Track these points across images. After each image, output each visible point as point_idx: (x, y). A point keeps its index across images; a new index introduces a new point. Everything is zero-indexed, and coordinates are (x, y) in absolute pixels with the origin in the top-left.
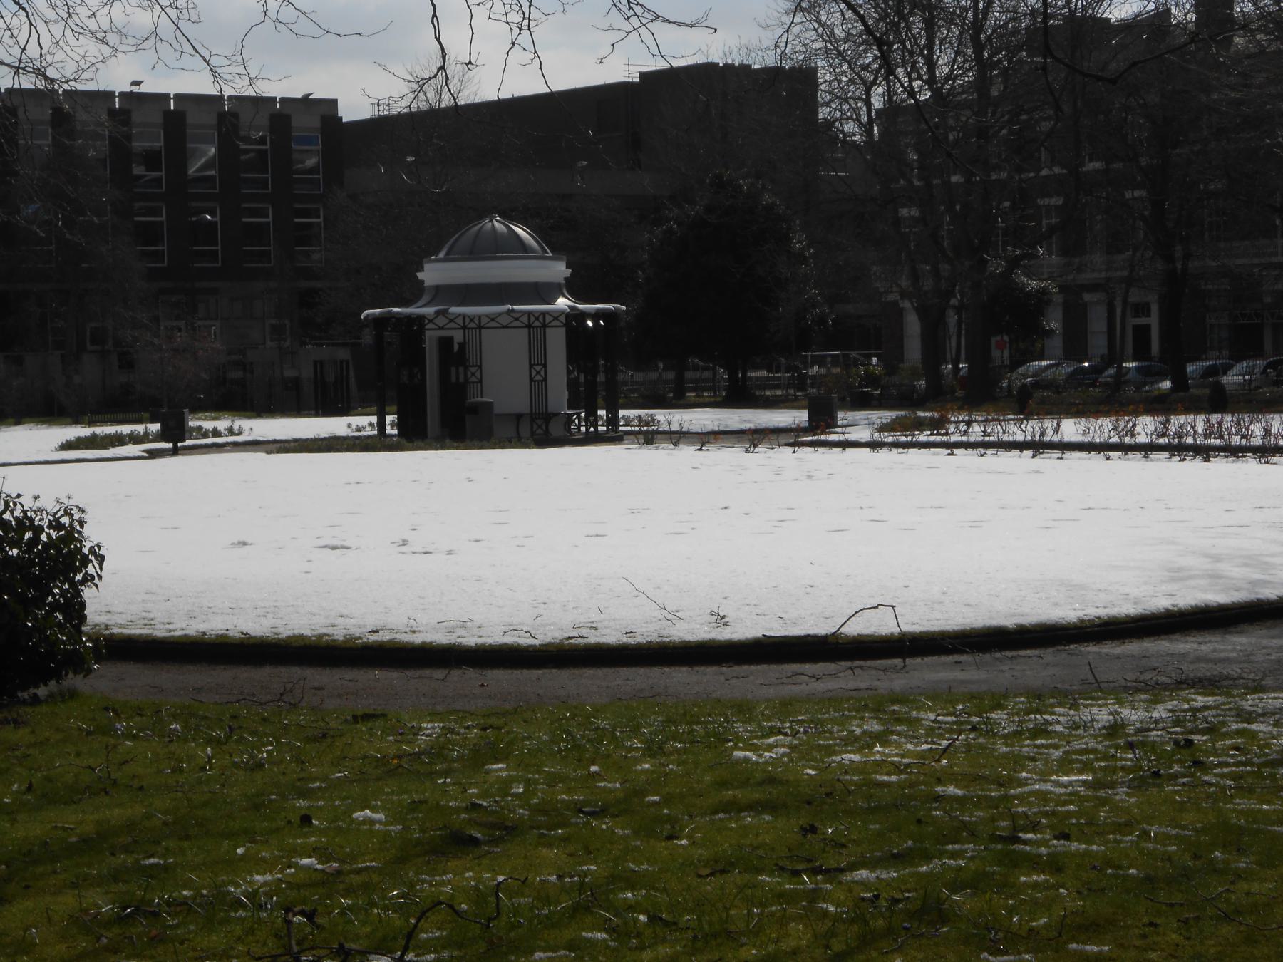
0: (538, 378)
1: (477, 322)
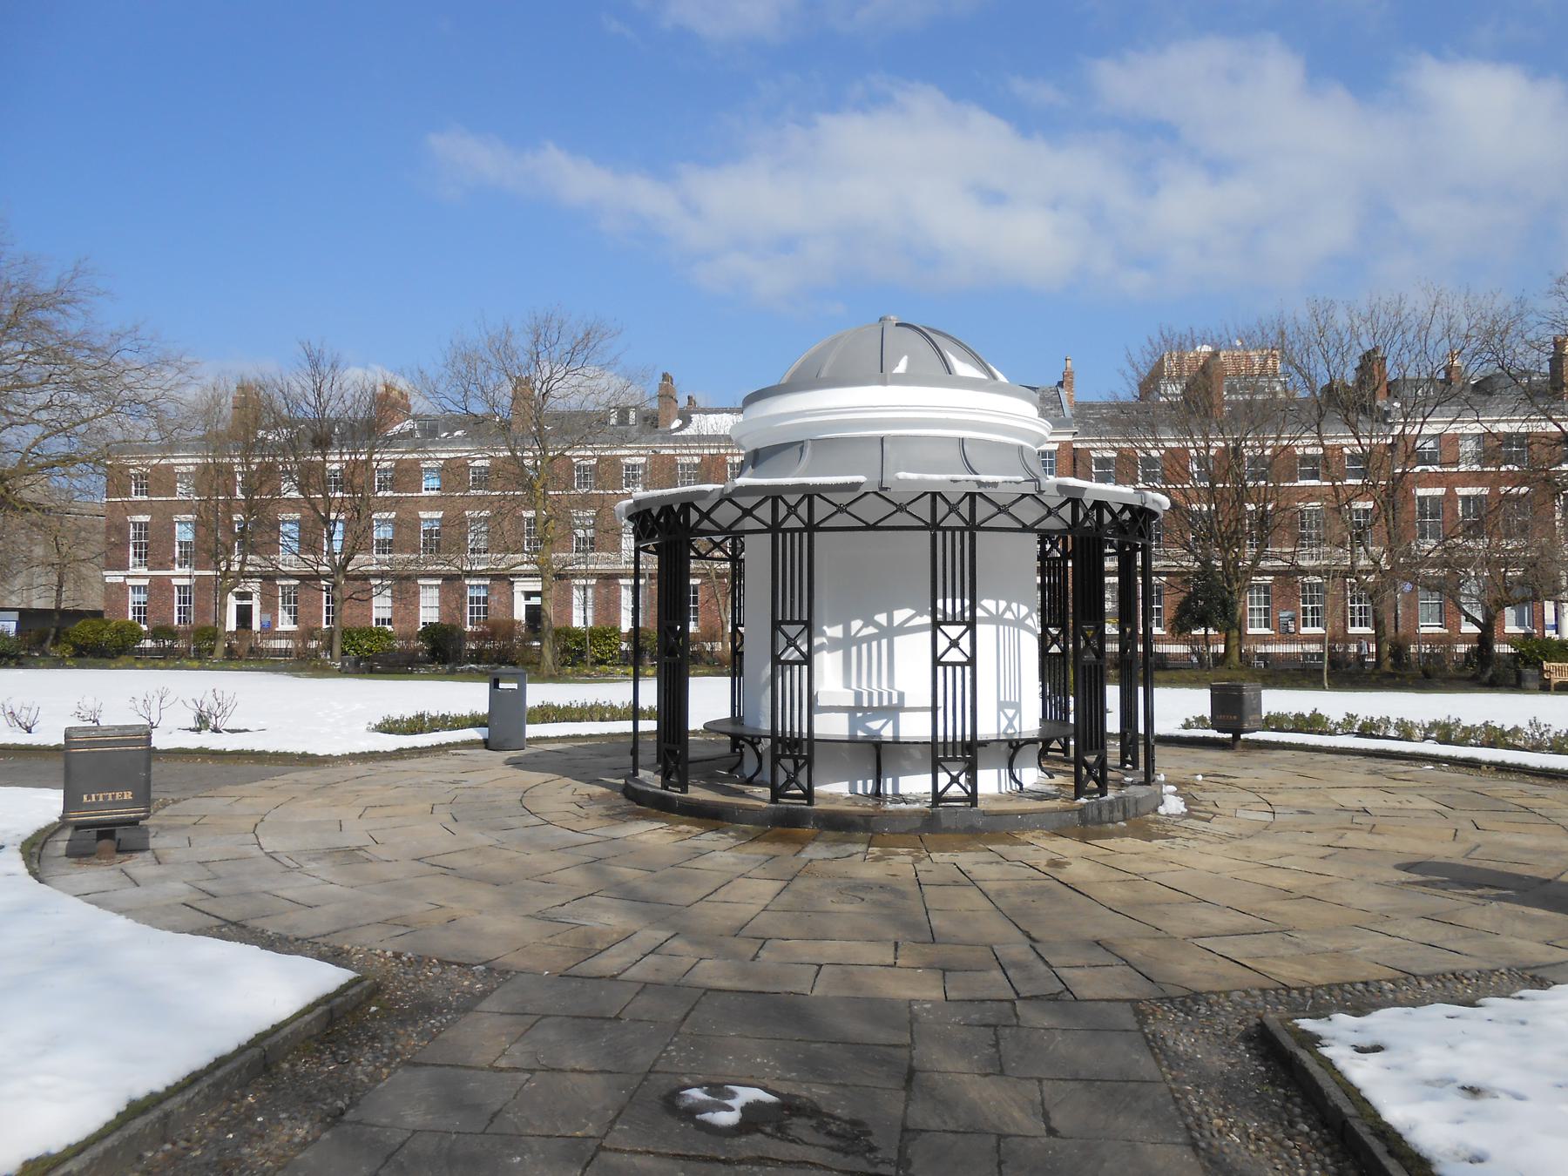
0: (954, 656)
1: (966, 513)
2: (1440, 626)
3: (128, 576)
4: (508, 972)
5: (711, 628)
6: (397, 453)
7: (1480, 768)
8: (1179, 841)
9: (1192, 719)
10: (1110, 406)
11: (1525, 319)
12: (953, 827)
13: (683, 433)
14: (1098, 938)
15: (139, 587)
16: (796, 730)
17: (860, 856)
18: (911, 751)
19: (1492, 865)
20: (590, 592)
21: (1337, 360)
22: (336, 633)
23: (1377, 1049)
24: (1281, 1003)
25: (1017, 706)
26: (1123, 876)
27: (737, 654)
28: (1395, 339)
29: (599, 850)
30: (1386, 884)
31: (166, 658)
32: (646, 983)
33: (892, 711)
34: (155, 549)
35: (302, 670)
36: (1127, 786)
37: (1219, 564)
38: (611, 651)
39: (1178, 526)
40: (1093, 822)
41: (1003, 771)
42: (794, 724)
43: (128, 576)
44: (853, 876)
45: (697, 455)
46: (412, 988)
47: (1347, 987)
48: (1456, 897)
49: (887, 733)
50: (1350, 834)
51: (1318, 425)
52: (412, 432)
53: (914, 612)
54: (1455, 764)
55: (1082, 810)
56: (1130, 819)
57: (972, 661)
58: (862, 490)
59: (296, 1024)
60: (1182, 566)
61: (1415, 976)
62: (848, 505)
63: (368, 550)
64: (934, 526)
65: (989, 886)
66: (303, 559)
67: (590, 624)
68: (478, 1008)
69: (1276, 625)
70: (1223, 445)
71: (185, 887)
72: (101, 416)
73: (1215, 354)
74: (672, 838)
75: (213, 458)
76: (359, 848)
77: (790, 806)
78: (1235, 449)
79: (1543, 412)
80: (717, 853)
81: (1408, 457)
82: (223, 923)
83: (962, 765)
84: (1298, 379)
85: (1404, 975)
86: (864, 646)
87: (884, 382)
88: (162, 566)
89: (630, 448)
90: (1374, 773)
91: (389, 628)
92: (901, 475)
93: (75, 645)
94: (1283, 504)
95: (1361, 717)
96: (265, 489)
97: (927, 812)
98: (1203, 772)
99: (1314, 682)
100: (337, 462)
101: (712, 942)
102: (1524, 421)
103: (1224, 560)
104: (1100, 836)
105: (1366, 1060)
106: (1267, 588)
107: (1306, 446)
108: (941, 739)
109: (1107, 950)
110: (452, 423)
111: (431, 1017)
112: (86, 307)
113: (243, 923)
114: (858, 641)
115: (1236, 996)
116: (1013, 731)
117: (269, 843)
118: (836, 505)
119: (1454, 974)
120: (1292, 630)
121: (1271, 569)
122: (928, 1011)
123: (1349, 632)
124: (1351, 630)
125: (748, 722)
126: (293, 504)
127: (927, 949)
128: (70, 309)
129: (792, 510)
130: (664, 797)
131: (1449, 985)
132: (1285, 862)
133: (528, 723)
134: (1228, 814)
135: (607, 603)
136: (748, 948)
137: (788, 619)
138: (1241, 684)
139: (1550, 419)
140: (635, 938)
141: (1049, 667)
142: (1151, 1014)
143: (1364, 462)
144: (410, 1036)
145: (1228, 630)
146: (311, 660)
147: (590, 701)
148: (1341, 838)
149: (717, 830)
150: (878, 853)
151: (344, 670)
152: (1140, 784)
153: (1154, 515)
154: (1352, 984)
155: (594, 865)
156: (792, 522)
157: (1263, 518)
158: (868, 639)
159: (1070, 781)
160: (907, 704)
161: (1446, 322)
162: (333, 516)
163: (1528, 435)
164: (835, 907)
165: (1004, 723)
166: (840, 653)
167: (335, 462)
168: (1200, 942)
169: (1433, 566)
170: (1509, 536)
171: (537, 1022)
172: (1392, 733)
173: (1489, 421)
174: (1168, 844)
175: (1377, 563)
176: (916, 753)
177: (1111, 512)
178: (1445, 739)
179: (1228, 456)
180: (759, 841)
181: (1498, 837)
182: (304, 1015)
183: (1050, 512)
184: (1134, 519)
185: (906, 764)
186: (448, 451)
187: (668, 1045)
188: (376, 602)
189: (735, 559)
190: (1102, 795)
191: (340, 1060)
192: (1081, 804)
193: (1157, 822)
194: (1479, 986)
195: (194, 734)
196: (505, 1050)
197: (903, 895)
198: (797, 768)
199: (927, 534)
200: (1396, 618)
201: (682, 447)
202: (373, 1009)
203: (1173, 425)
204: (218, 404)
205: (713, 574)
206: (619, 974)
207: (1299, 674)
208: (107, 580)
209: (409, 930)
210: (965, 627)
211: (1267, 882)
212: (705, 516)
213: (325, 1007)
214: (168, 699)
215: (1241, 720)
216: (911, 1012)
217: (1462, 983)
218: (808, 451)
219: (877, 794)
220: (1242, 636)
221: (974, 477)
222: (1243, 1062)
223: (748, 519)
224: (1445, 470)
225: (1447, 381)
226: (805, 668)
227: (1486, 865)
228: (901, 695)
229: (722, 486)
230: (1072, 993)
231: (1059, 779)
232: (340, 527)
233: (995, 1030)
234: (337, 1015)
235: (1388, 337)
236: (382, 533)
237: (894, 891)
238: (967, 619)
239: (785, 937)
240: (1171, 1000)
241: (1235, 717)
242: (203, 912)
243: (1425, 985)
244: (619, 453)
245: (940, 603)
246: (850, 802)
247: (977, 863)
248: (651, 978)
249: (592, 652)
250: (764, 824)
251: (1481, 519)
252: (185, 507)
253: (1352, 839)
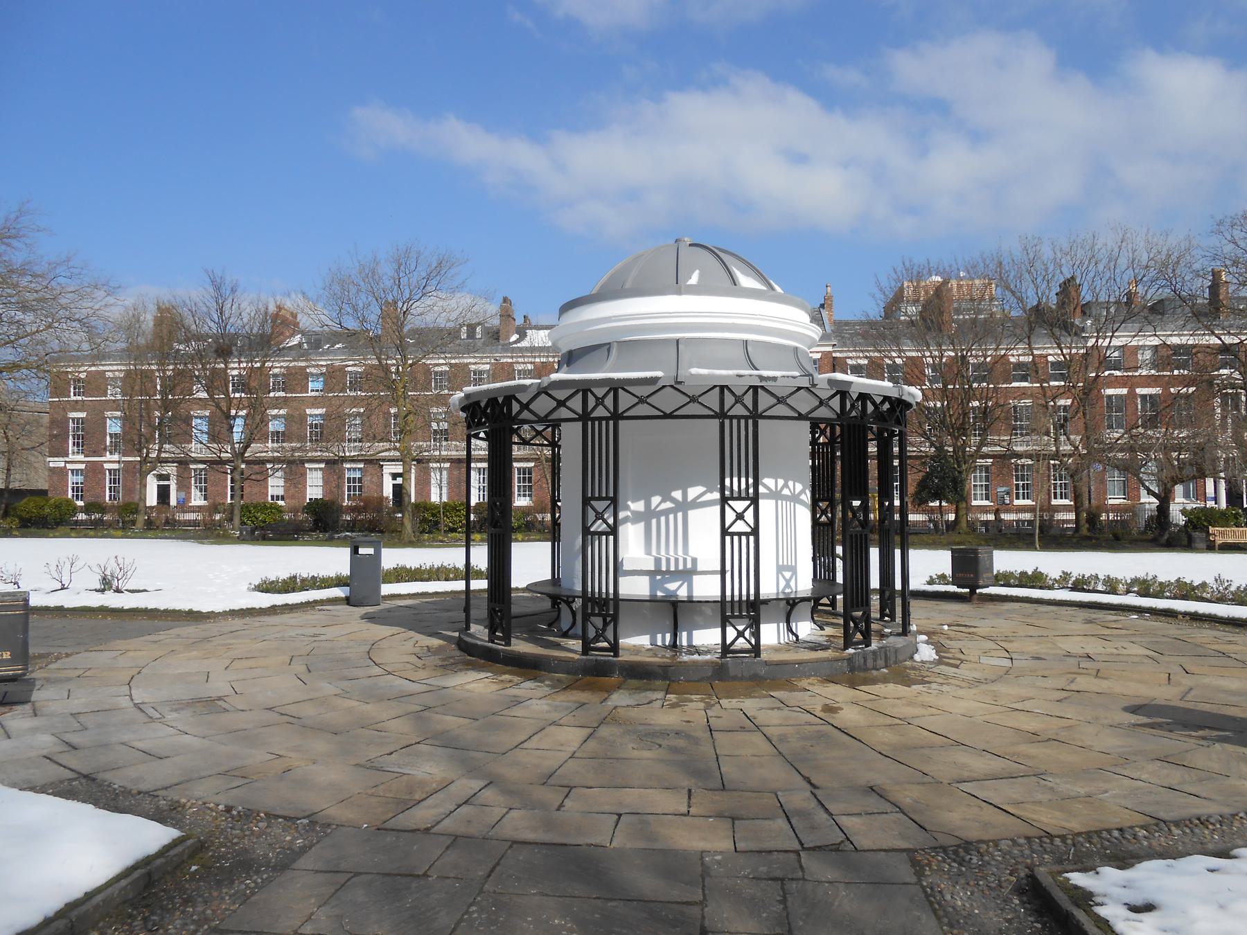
0: (740, 527)
2: (1124, 499)
3: (69, 462)
4: (329, 825)
5: (542, 502)
6: (284, 361)
7: (1176, 617)
8: (934, 686)
9: (935, 577)
10: (862, 323)
11: (1193, 253)
12: (740, 675)
13: (519, 345)
14: (872, 784)
15: (77, 470)
16: (604, 590)
17: (659, 703)
18: (703, 608)
19: (1207, 708)
20: (445, 473)
21: (1044, 286)
22: (236, 508)
23: (1148, 908)
24: (1045, 851)
25: (793, 570)
26: (889, 721)
27: (556, 523)
28: (1090, 268)
29: (428, 700)
30: (1118, 726)
31: (96, 528)
32: (456, 837)
33: (687, 574)
34: (90, 439)
35: (207, 538)
36: (887, 636)
37: (951, 449)
38: (460, 521)
39: (917, 419)
40: (859, 669)
41: (781, 624)
42: (602, 585)
43: (69, 462)
44: (652, 722)
45: (531, 363)
46: (236, 844)
47: (1105, 834)
48: (1184, 739)
49: (683, 593)
50: (1079, 679)
51: (1029, 338)
52: (300, 345)
53: (705, 489)
54: (1155, 614)
55: (850, 659)
56: (891, 666)
57: (755, 531)
58: (660, 384)
59: (110, 890)
60: (921, 451)
61: (1164, 822)
62: (648, 397)
63: (264, 439)
64: (722, 415)
65: (773, 732)
66: (208, 447)
67: (445, 499)
68: (295, 866)
69: (994, 497)
70: (953, 354)
71: (52, 739)
72: (41, 331)
73: (945, 282)
74: (494, 687)
75: (135, 365)
76: (220, 699)
77: (599, 658)
78: (963, 357)
79: (1207, 328)
80: (534, 701)
81: (1100, 363)
82: (74, 775)
83: (746, 621)
84: (1013, 300)
85: (1154, 821)
86: (663, 519)
87: (679, 292)
88: (95, 454)
89: (475, 357)
90: (1089, 622)
91: (281, 503)
92: (694, 371)
93: (21, 519)
94: (1001, 402)
95: (1075, 575)
96: (178, 390)
97: (717, 663)
98: (948, 622)
99: (1027, 544)
100: (236, 368)
101: (516, 795)
102: (1191, 335)
103: (954, 446)
104: (866, 682)
105: (1141, 921)
106: (987, 468)
107: (1018, 355)
108: (729, 599)
109: (881, 796)
110: (334, 337)
111: (249, 877)
112: (28, 241)
113: (94, 776)
114: (658, 514)
115: (1004, 845)
116: (790, 591)
117: (139, 696)
118: (637, 397)
119: (1199, 819)
120: (1008, 502)
121: (991, 453)
122: (718, 863)
123: (1052, 503)
124: (1054, 502)
125: (564, 584)
126: (202, 403)
127: (717, 797)
128: (14, 243)
129: (600, 401)
130: (490, 650)
131: (1197, 831)
132: (1027, 705)
133: (383, 583)
134: (973, 660)
136: (554, 797)
137: (597, 495)
138: (976, 547)
139: (1213, 333)
140: (452, 788)
141: (822, 536)
142: (927, 865)
143: (1064, 368)
144: (223, 899)
145: (958, 502)
146: (216, 529)
147: (437, 564)
148: (1072, 682)
149: (534, 679)
150: (675, 700)
151: (242, 538)
152: (898, 635)
153: (909, 405)
154: (1109, 831)
155: (418, 717)
156: (600, 412)
157: (985, 412)
158: (666, 513)
159: (840, 632)
160: (700, 568)
161: (1131, 256)
162: (233, 412)
163: (1194, 346)
164: (636, 754)
165: (782, 583)
166: (642, 525)
167: (236, 368)
168: (964, 787)
169: (1121, 450)
170: (1180, 427)
171: (348, 880)
172: (1100, 588)
173: (1164, 335)
174: (925, 689)
175: (1076, 448)
176: (708, 610)
177: (874, 403)
178: (1144, 593)
179: (957, 362)
180: (572, 689)
181: (1206, 681)
182: (121, 879)
183: (821, 403)
184: (892, 410)
185: (699, 619)
186: (326, 360)
187: (471, 905)
188: (271, 481)
189: (554, 444)
190: (867, 646)
191: (150, 927)
192: (850, 654)
193: (914, 668)
194: (1223, 831)
195: (99, 595)
196: (312, 914)
197: (696, 741)
198: (605, 624)
199: (716, 422)
200: (1089, 492)
201: (517, 357)
202: (194, 868)
203: (912, 338)
204: (138, 321)
205: (543, 458)
206: (433, 827)
207: (1019, 538)
208: (51, 465)
209: (247, 781)
210: (749, 502)
211: (1016, 725)
212: (525, 407)
213: (143, 871)
214: (78, 564)
215: (977, 577)
216: (703, 864)
217: (1208, 828)
218: (614, 352)
219: (674, 645)
220: (969, 508)
221: (756, 372)
222: (1019, 917)
223: (563, 409)
224: (1130, 374)
225: (1129, 302)
226: (611, 538)
227: (1201, 707)
228: (694, 561)
229: (539, 381)
230: (852, 843)
231: (829, 630)
232: (239, 422)
233: (783, 884)
234: (156, 877)
235: (1085, 267)
236: (274, 426)
237: (688, 737)
238: (751, 495)
239: (589, 785)
240: (945, 849)
241: (972, 576)
242: (61, 765)
243: (1176, 831)
244: (466, 361)
245: (727, 482)
246: (651, 654)
247: (761, 709)
248: (462, 830)
249: (445, 522)
250: (575, 674)
251: (1157, 412)
252: (115, 405)
253: (1082, 683)
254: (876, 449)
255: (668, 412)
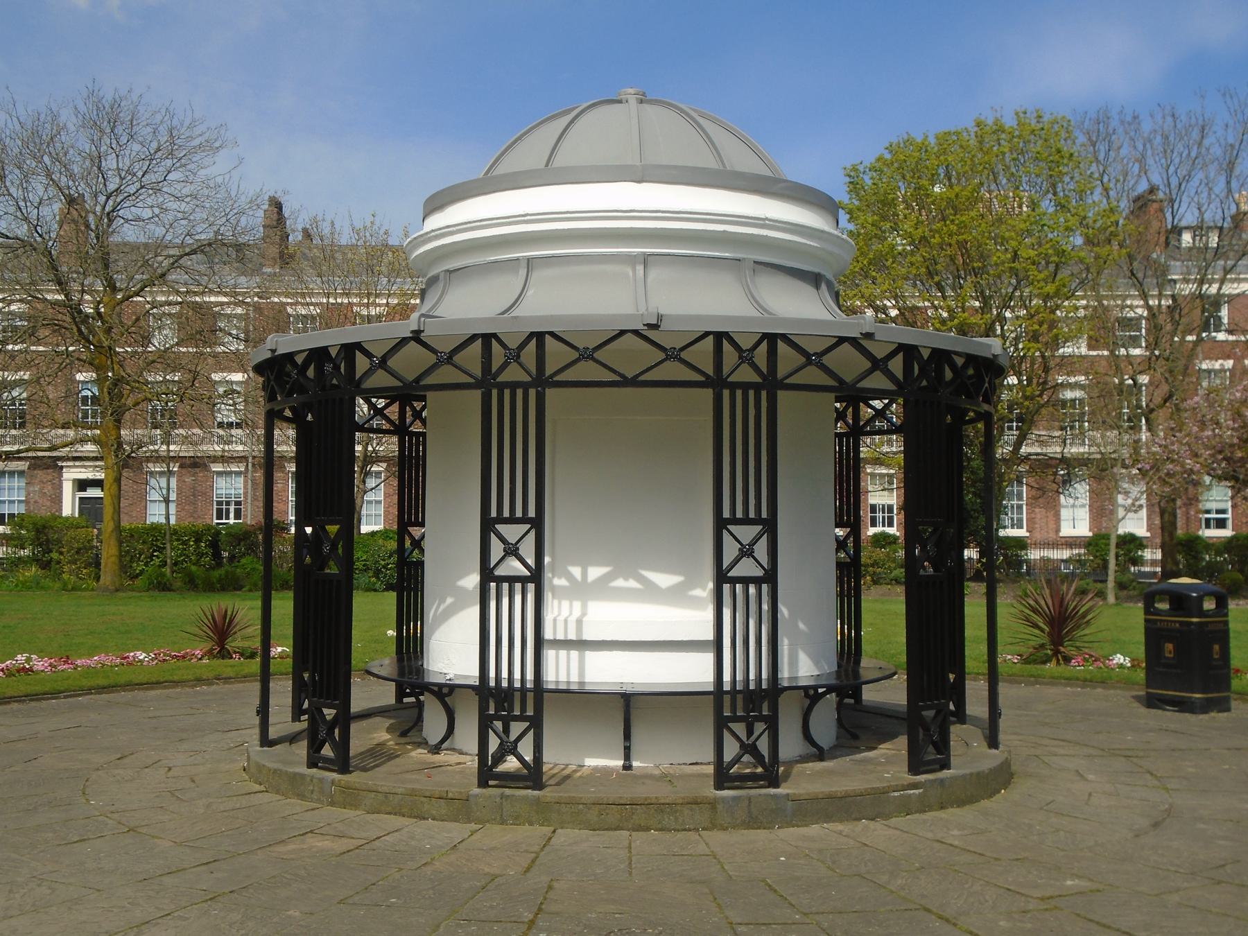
57: (770, 577)
135: (194, 495)
156: (513, 374)
177: (953, 366)
254: (861, 449)
255: (630, 375)
